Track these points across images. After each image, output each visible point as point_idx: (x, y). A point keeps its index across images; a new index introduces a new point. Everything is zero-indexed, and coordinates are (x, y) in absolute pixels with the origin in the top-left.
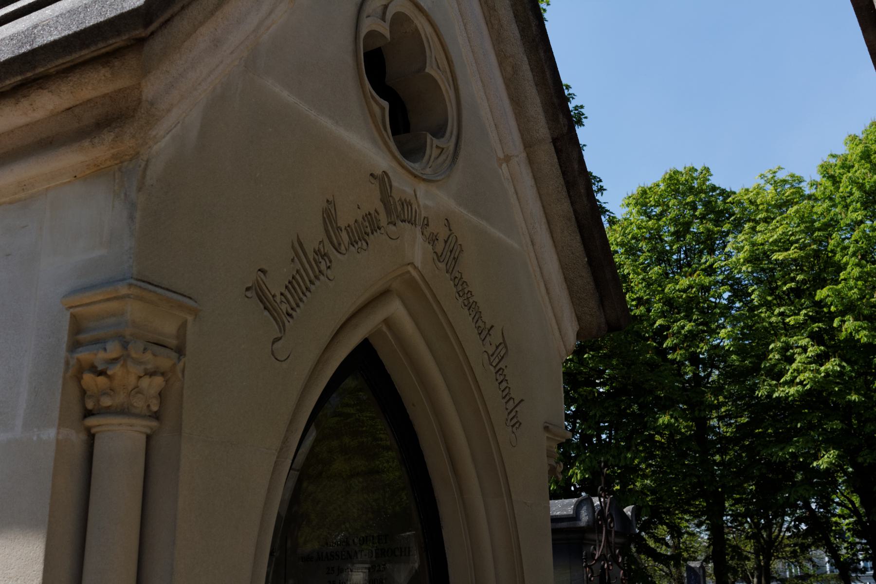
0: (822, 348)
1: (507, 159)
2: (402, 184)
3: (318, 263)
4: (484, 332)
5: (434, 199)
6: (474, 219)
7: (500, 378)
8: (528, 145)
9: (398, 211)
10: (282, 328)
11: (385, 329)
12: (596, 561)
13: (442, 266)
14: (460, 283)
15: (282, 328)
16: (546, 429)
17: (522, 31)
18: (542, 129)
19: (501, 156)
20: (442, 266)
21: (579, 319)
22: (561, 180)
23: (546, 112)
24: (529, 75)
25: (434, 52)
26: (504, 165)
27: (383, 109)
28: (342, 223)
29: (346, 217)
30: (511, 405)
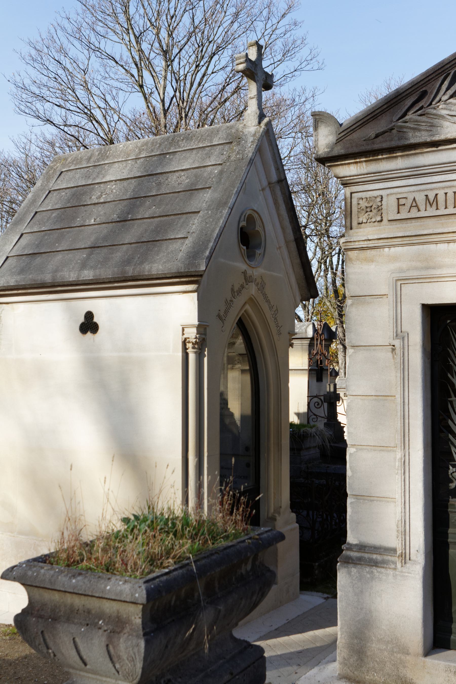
0: (33, 651)
1: (280, 248)
2: (249, 272)
3: (230, 303)
4: (271, 308)
5: (257, 272)
6: (269, 272)
7: (275, 321)
8: (287, 242)
9: (248, 279)
10: (223, 323)
11: (245, 314)
12: (314, 356)
13: (260, 292)
14: (265, 295)
15: (223, 323)
16: (289, 333)
17: (286, 207)
18: (291, 237)
19: (278, 247)
20: (260, 292)
21: (301, 295)
22: (297, 252)
23: (293, 231)
24: (286, 638)
25: (258, 222)
26: (279, 250)
27: (244, 250)
28: (235, 290)
29: (236, 289)
30: (279, 328)
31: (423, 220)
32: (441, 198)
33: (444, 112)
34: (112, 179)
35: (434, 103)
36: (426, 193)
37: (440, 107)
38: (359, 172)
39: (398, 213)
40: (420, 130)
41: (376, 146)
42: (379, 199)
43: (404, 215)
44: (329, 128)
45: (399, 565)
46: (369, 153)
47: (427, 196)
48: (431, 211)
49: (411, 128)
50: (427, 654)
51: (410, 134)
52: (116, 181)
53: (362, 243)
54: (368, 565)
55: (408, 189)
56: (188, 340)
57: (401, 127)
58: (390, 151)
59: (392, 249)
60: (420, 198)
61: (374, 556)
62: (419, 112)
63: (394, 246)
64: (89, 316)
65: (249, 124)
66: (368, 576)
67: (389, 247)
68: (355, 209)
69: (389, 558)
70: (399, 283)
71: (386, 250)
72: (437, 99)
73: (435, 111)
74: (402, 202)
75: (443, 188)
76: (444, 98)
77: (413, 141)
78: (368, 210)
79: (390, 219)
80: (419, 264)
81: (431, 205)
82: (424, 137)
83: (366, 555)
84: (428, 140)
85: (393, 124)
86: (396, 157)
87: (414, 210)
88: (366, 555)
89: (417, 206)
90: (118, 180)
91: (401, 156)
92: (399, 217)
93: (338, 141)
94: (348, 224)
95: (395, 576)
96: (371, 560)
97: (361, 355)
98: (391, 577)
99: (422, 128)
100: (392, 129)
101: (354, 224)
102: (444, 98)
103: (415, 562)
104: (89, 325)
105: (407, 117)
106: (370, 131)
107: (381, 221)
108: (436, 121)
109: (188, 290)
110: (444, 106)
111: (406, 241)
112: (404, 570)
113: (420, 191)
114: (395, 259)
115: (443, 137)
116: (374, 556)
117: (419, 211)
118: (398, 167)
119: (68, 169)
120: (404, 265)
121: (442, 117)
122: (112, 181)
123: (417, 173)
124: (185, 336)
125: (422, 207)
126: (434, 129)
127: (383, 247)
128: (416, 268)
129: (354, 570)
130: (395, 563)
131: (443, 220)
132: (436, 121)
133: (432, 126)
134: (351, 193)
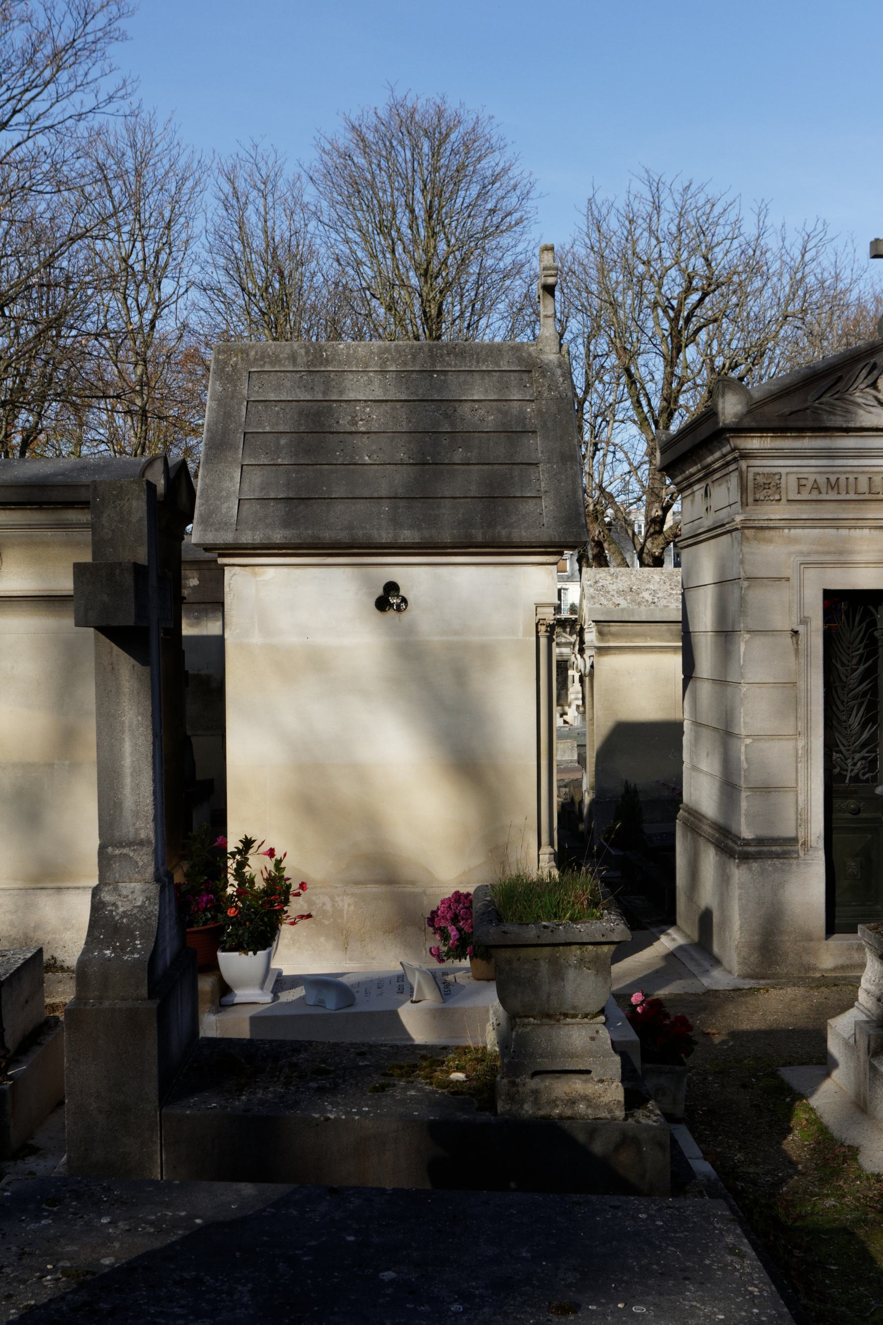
31: (823, 503)
32: (843, 482)
33: (860, 400)
34: (360, 398)
35: (851, 389)
36: (827, 476)
37: (857, 394)
38: (762, 447)
39: (799, 493)
40: (834, 414)
41: (791, 424)
42: (777, 477)
43: (805, 496)
44: (737, 397)
45: (801, 853)
46: (780, 430)
47: (828, 479)
48: (832, 496)
49: (826, 411)
50: (827, 939)
51: (825, 417)
52: (365, 401)
53: (762, 522)
54: (769, 858)
55: (810, 469)
56: (541, 622)
57: (817, 408)
58: (800, 431)
59: (793, 531)
60: (822, 480)
61: (774, 849)
62: (836, 396)
63: (795, 528)
64: (392, 588)
65: (547, 349)
66: (770, 869)
67: (790, 528)
68: (751, 485)
69: (789, 848)
70: (803, 566)
71: (786, 531)
72: (855, 386)
73: (852, 398)
74: (803, 482)
75: (845, 473)
76: (862, 386)
77: (828, 424)
78: (767, 486)
79: (790, 498)
80: (820, 548)
81: (832, 488)
82: (839, 422)
83: (765, 849)
84: (844, 426)
85: (809, 404)
86: (805, 437)
87: (815, 492)
88: (765, 849)
89: (818, 488)
90: (371, 401)
91: (810, 437)
92: (799, 497)
93: (749, 412)
94: (744, 501)
95: (798, 865)
96: (771, 852)
97: (759, 642)
98: (794, 866)
99: (838, 413)
100: (807, 409)
101: (750, 500)
102: (862, 386)
103: (816, 849)
104: (388, 599)
105: (823, 399)
106: (784, 407)
107: (780, 500)
108: (851, 408)
109: (548, 561)
110: (861, 394)
111: (809, 523)
112: (807, 857)
113: (820, 473)
114: (792, 541)
115: (858, 425)
116: (774, 849)
117: (820, 493)
118: (804, 447)
119: (259, 369)
120: (805, 548)
121: (858, 405)
122: (360, 401)
123: (831, 454)
124: (539, 617)
125: (824, 490)
126: (849, 415)
127: (783, 528)
128: (817, 552)
129: (755, 865)
130: (797, 852)
131: (844, 506)
132: (851, 408)
133: (848, 411)
134: (748, 467)
